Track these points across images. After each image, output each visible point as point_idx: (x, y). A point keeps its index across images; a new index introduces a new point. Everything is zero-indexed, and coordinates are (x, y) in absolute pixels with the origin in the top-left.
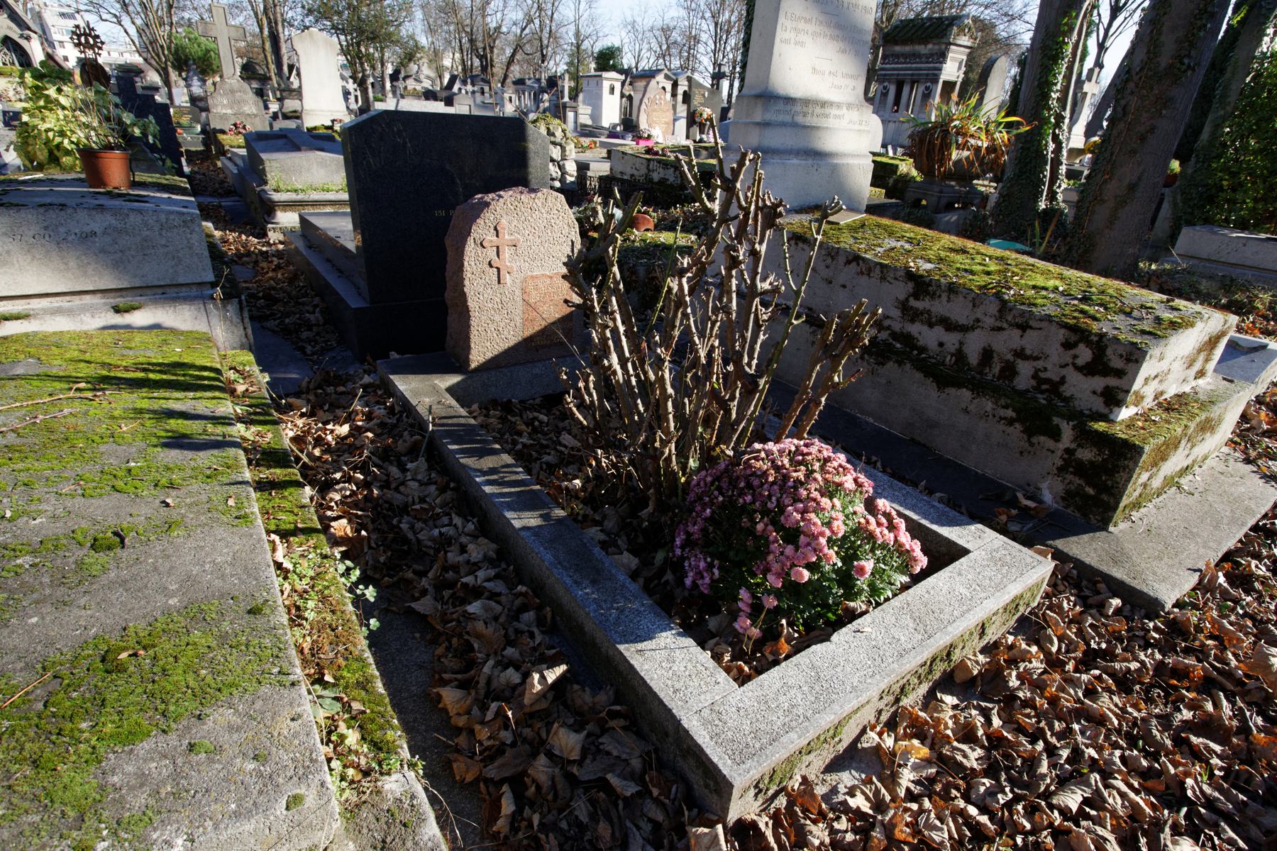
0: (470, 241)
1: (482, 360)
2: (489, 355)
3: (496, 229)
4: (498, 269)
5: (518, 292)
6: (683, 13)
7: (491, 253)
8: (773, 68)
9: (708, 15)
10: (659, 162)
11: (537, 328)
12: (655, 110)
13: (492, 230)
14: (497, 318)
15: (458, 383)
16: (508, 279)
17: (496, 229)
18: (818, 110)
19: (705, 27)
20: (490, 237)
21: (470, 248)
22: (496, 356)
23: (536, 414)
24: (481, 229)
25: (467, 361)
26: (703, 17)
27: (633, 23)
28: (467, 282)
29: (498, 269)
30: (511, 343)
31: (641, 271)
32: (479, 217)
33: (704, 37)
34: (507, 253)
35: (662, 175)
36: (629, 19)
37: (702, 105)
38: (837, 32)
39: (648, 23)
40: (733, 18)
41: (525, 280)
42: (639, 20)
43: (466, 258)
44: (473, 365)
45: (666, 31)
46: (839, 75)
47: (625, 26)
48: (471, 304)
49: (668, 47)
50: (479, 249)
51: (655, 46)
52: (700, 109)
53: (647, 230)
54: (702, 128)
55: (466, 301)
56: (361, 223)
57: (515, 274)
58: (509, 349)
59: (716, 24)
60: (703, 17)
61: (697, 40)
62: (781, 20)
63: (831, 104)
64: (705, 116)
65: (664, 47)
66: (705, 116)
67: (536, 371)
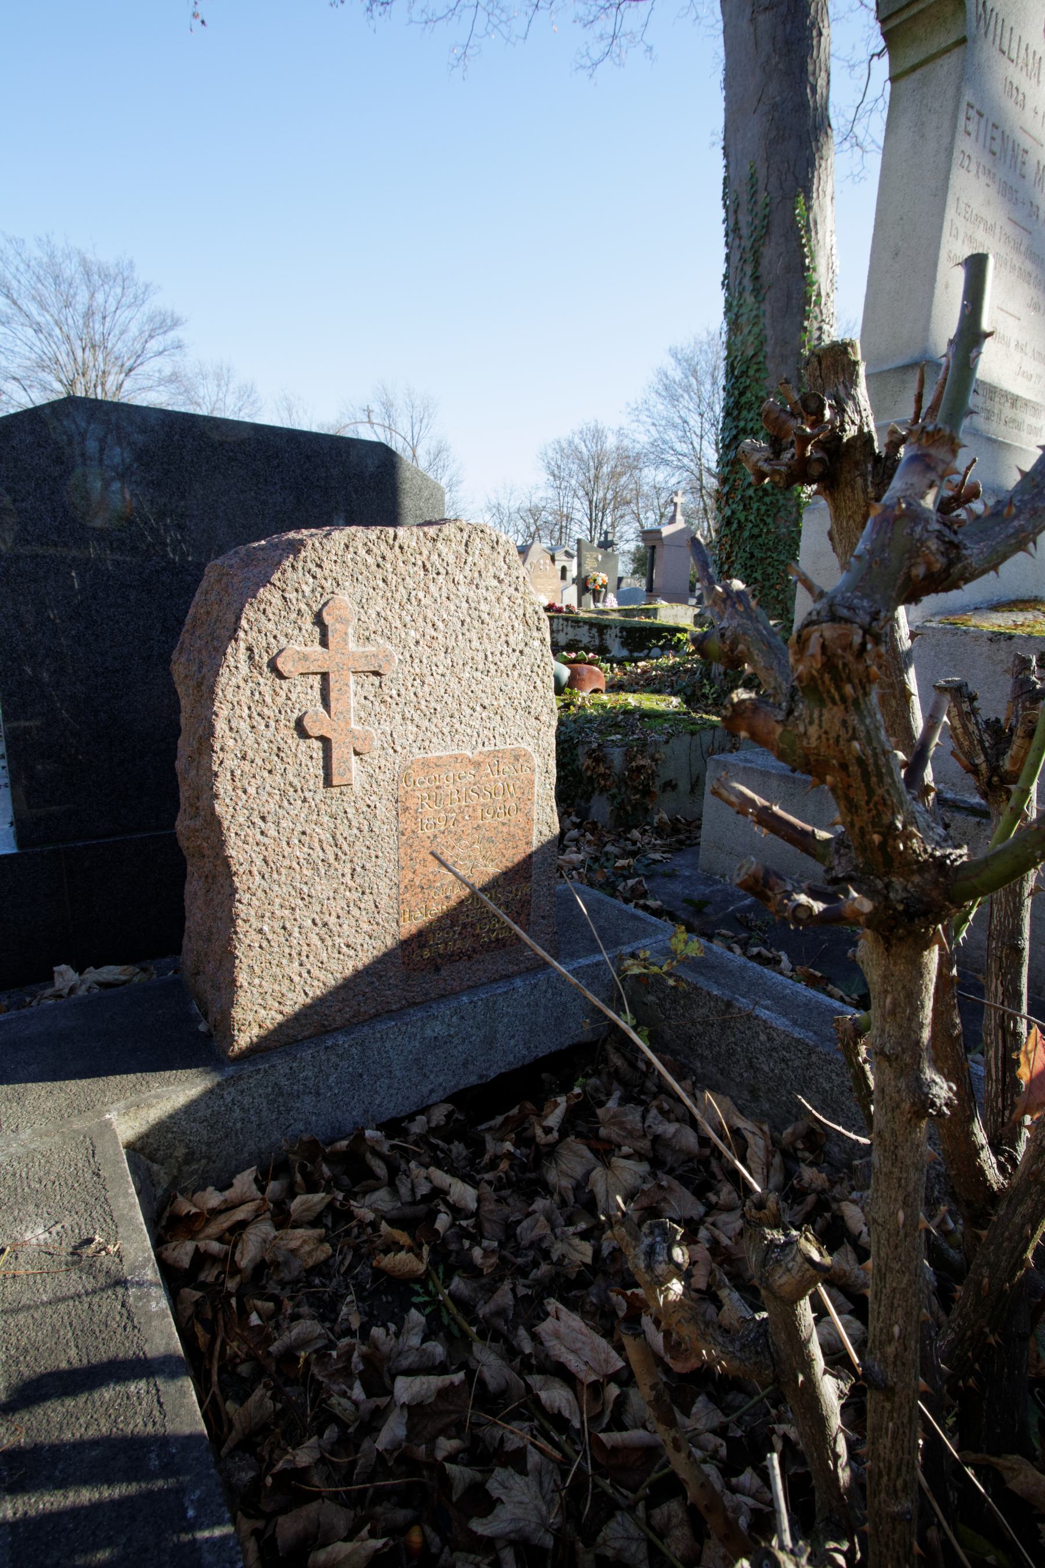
0: (236, 655)
1: (272, 1018)
2: (296, 1001)
3: (319, 620)
4: (325, 741)
5: (384, 810)
6: (551, 493)
7: (305, 695)
8: (935, 311)
9: (581, 493)
10: (566, 619)
11: (437, 908)
12: (539, 577)
13: (307, 623)
14: (322, 888)
15: (190, 1109)
16: (352, 771)
17: (319, 620)
18: (1008, 412)
19: (577, 504)
20: (300, 649)
21: (236, 683)
22: (320, 1002)
23: (441, 1178)
24: (271, 620)
25: (225, 1027)
26: (575, 495)
27: (498, 508)
28: (223, 785)
29: (325, 741)
30: (364, 958)
31: (617, 756)
32: (265, 581)
33: (577, 515)
34: (351, 694)
35: (571, 637)
36: (494, 502)
37: (595, 569)
38: (1029, 266)
39: (514, 505)
40: (609, 496)
41: (404, 777)
42: (504, 503)
43: (223, 710)
44: (243, 1039)
45: (534, 512)
46: (1029, 350)
47: (490, 509)
48: (235, 850)
49: (538, 529)
50: (266, 682)
51: (521, 526)
52: (593, 574)
53: (596, 691)
54: (596, 595)
55: (221, 844)
56: (1032, 1081)
57: (374, 757)
58: (358, 974)
59: (591, 502)
60: (575, 495)
61: (569, 518)
62: (950, 214)
63: (1026, 403)
64: (600, 582)
65: (533, 529)
66: (600, 582)
67: (436, 1029)
